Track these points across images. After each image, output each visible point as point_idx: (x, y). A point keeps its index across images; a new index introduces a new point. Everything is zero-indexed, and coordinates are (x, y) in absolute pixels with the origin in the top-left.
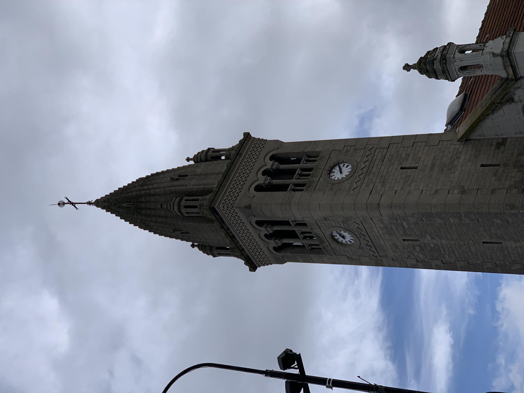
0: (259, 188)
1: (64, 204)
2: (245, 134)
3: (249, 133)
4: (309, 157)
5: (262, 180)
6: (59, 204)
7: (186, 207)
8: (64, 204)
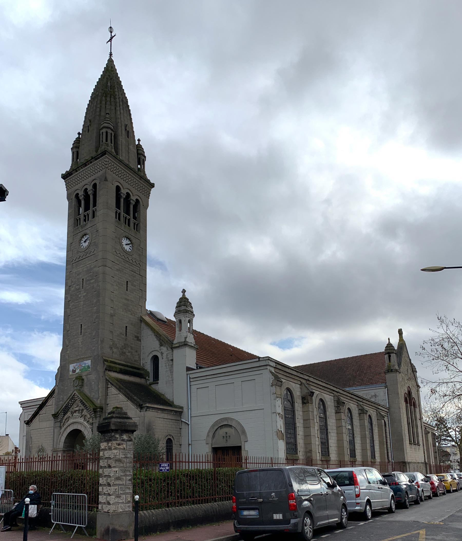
0: (118, 188)
1: (111, 32)
2: (154, 184)
3: (154, 187)
4: (137, 225)
5: (124, 192)
6: (111, 27)
7: (107, 133)
8: (111, 32)
